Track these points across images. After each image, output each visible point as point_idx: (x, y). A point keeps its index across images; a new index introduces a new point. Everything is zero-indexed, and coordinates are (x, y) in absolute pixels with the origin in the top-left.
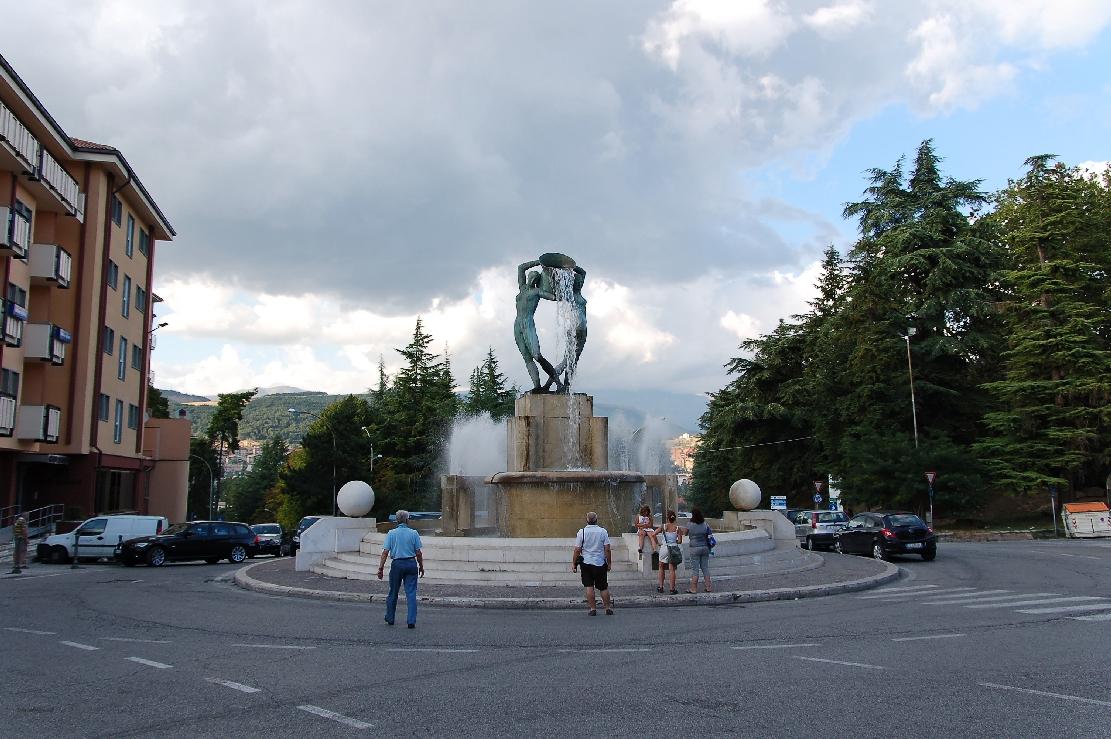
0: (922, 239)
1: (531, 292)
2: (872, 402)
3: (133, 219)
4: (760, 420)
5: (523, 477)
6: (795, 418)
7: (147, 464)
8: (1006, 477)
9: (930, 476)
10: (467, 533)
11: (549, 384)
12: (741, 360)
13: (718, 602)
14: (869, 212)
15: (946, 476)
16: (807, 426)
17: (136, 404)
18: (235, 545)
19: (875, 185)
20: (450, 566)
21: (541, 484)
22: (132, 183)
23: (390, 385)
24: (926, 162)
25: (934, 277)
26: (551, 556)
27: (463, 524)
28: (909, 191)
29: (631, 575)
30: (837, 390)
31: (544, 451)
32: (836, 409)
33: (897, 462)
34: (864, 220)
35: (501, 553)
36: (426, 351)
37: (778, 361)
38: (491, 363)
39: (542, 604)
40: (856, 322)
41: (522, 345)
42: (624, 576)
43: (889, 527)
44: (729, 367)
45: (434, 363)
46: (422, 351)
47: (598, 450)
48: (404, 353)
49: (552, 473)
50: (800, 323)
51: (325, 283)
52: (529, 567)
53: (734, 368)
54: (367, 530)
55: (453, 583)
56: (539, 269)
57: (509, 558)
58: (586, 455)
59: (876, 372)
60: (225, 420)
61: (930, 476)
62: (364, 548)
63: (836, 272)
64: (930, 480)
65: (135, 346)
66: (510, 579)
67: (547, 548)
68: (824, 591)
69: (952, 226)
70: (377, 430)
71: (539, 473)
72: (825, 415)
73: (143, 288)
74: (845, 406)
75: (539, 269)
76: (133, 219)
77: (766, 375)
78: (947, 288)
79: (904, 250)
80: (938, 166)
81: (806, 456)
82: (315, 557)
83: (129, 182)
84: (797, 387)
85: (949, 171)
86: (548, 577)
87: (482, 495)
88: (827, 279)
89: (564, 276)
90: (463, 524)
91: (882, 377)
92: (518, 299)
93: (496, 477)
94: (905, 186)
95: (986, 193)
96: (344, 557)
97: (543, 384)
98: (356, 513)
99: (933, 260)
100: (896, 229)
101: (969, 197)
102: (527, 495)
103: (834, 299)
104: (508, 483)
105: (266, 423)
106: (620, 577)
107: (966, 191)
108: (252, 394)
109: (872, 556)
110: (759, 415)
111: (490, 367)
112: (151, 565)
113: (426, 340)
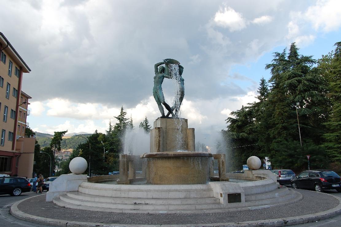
0: (295, 74)
1: (161, 75)
3: (12, 63)
5: (156, 155)
6: (250, 138)
7: (18, 154)
8: (336, 156)
9: (308, 157)
10: (131, 182)
11: (168, 115)
12: (231, 118)
14: (274, 67)
15: (315, 156)
17: (12, 131)
18: (14, 189)
19: (276, 58)
20: (118, 201)
21: (168, 158)
22: (9, 46)
23: (113, 129)
24: (294, 50)
25: (300, 87)
27: (131, 176)
28: (287, 60)
29: (217, 206)
30: (268, 127)
32: (268, 134)
33: (295, 151)
34: (272, 70)
35: (145, 193)
36: (124, 117)
38: (146, 121)
41: (156, 97)
42: (213, 206)
43: (322, 176)
44: (227, 120)
46: (123, 117)
47: (190, 143)
48: (117, 118)
49: (171, 153)
50: (250, 106)
51: (98, 101)
52: (160, 202)
54: (82, 181)
55: (119, 212)
56: (164, 65)
57: (150, 196)
58: (186, 146)
59: (283, 120)
60: (56, 141)
61: (308, 157)
62: (81, 189)
64: (308, 158)
65: (12, 110)
66: (149, 209)
67: (169, 191)
68: (329, 216)
69: (305, 70)
70: (108, 144)
71: (165, 153)
72: (263, 136)
73: (17, 89)
75: (164, 65)
76: (12, 63)
77: (240, 123)
78: (305, 91)
79: (289, 79)
80: (298, 51)
81: (254, 151)
82: (55, 195)
83: (8, 46)
84: (251, 127)
85: (302, 53)
86: (171, 208)
88: (262, 89)
89: (175, 67)
90: (131, 176)
91: (286, 121)
92: (155, 78)
93: (145, 155)
94: (286, 58)
95: (314, 60)
96: (69, 195)
97: (166, 115)
99: (299, 82)
100: (285, 72)
101: (309, 61)
102: (160, 163)
103: (264, 96)
104: (150, 157)
105: (77, 144)
107: (307, 59)
109: (315, 190)
112: (12, 195)
113: (124, 114)
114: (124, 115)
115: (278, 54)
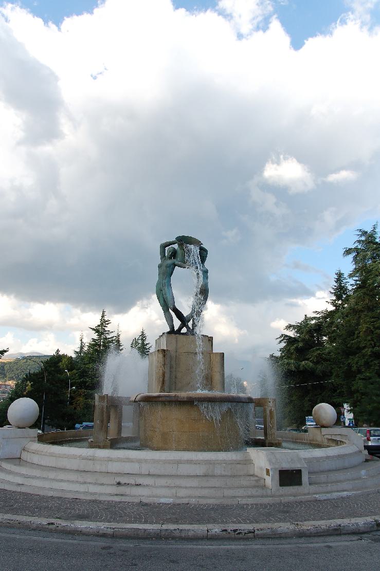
1: (170, 262)
2: (372, 359)
4: (298, 371)
5: (159, 397)
10: (114, 444)
11: (180, 329)
12: (287, 336)
13: (362, 529)
14: (358, 253)
16: (326, 375)
20: (89, 478)
23: (86, 349)
26: (184, 469)
29: (260, 492)
30: (349, 352)
31: (176, 378)
34: (355, 258)
35: (137, 465)
36: (106, 329)
37: (307, 337)
39: (177, 534)
40: (359, 311)
42: (254, 492)
45: (111, 335)
47: (217, 377)
48: (93, 329)
49: (183, 395)
50: (318, 316)
52: (162, 482)
53: (282, 340)
54: (29, 439)
56: (176, 246)
57: (144, 471)
62: (25, 456)
63: (343, 285)
67: (179, 462)
70: (77, 373)
71: (173, 394)
74: (355, 362)
75: (176, 246)
77: (301, 345)
86: (182, 493)
87: (128, 411)
88: (337, 289)
90: (112, 435)
92: (160, 266)
97: (176, 328)
98: (21, 426)
102: (160, 412)
103: (342, 300)
104: (148, 399)
105: (23, 372)
106: (250, 493)
108: (5, 351)
110: (298, 367)
111: (142, 339)
113: (107, 323)
114: (106, 325)
115: (365, 233)
